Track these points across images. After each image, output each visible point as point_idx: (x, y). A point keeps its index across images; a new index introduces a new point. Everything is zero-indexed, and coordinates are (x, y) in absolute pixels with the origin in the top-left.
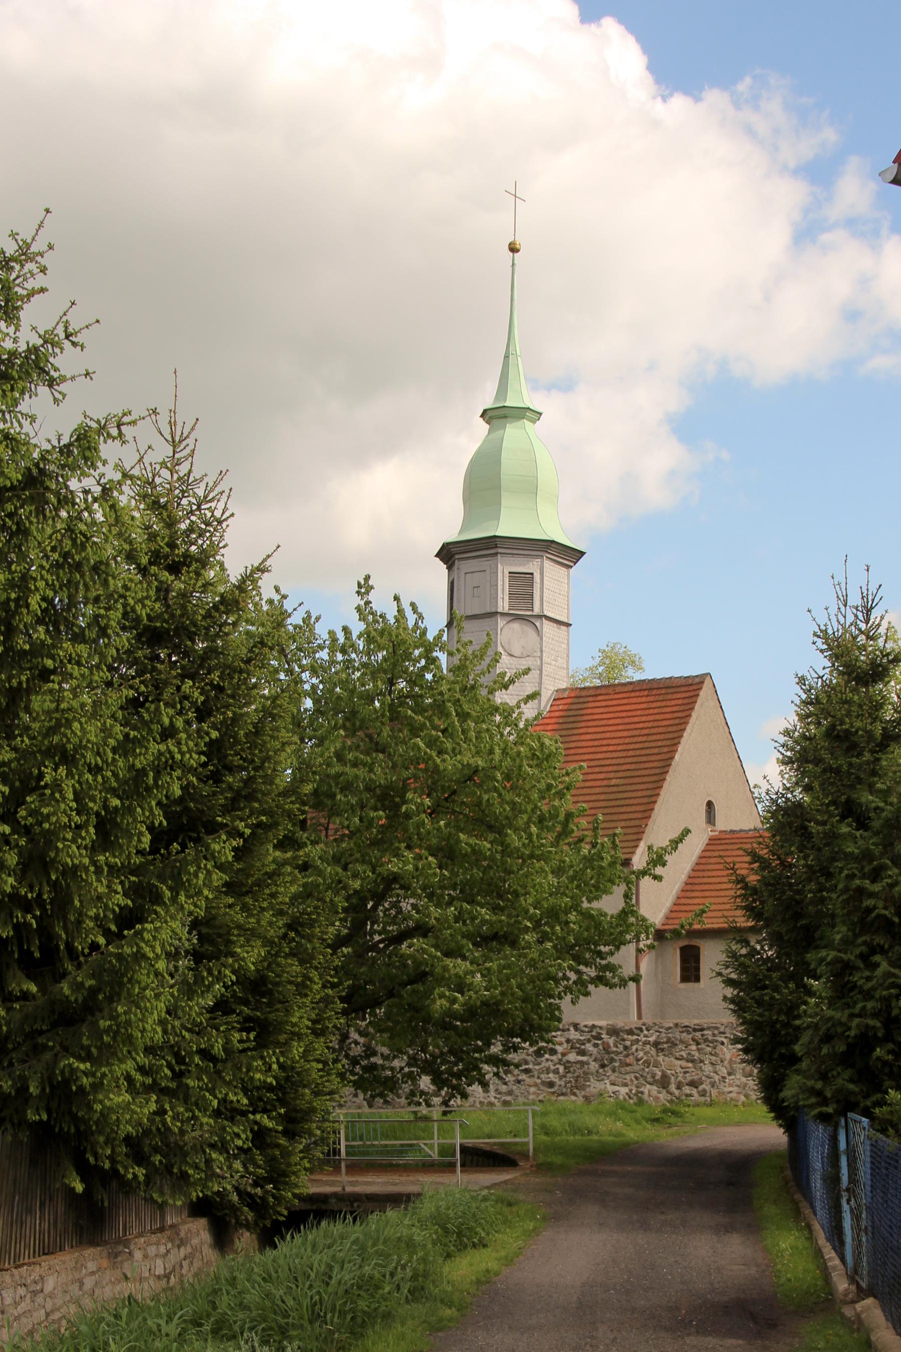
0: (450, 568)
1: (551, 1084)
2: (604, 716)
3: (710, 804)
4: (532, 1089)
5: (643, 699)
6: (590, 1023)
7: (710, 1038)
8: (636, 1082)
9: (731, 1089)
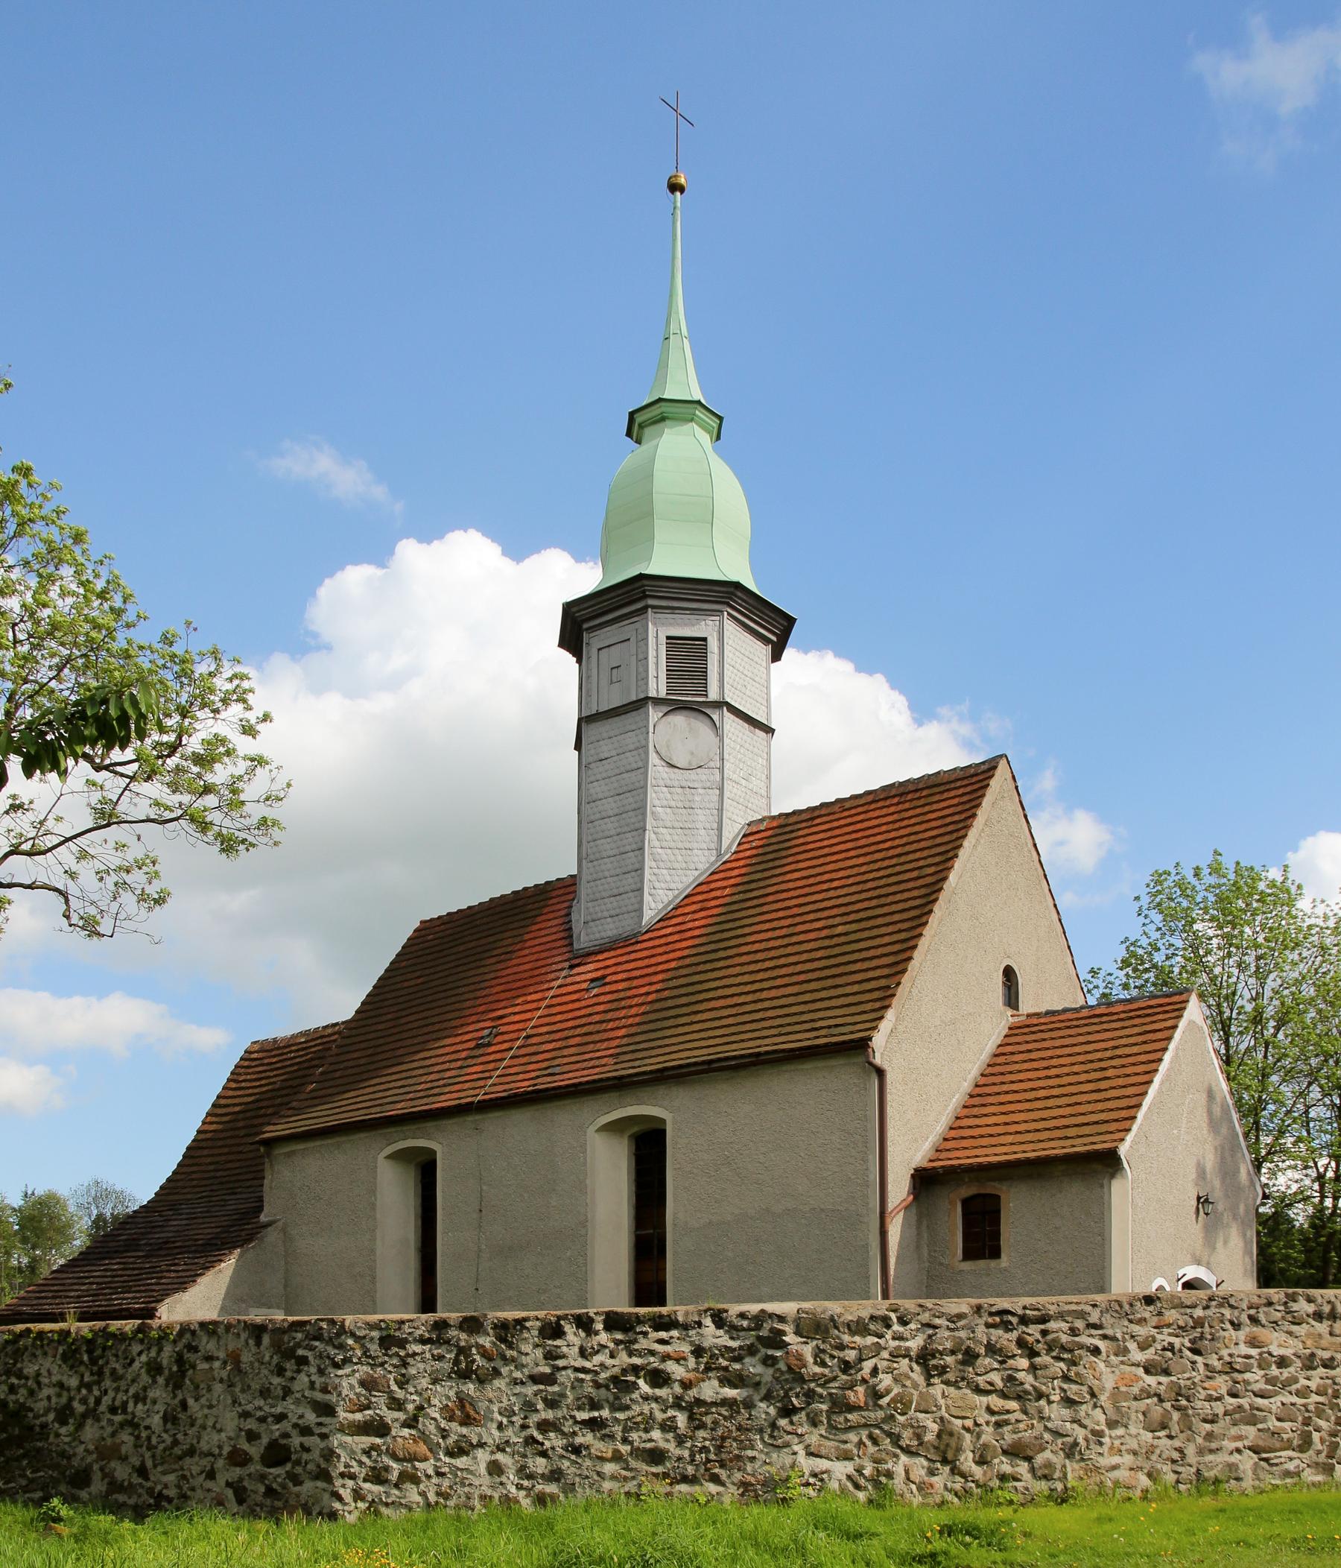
0: (579, 661)
1: (656, 1456)
2: (826, 843)
3: (1009, 973)
4: (609, 1468)
5: (892, 809)
6: (754, 1308)
7: (1064, 1338)
8: (872, 1449)
9: (1116, 1460)
